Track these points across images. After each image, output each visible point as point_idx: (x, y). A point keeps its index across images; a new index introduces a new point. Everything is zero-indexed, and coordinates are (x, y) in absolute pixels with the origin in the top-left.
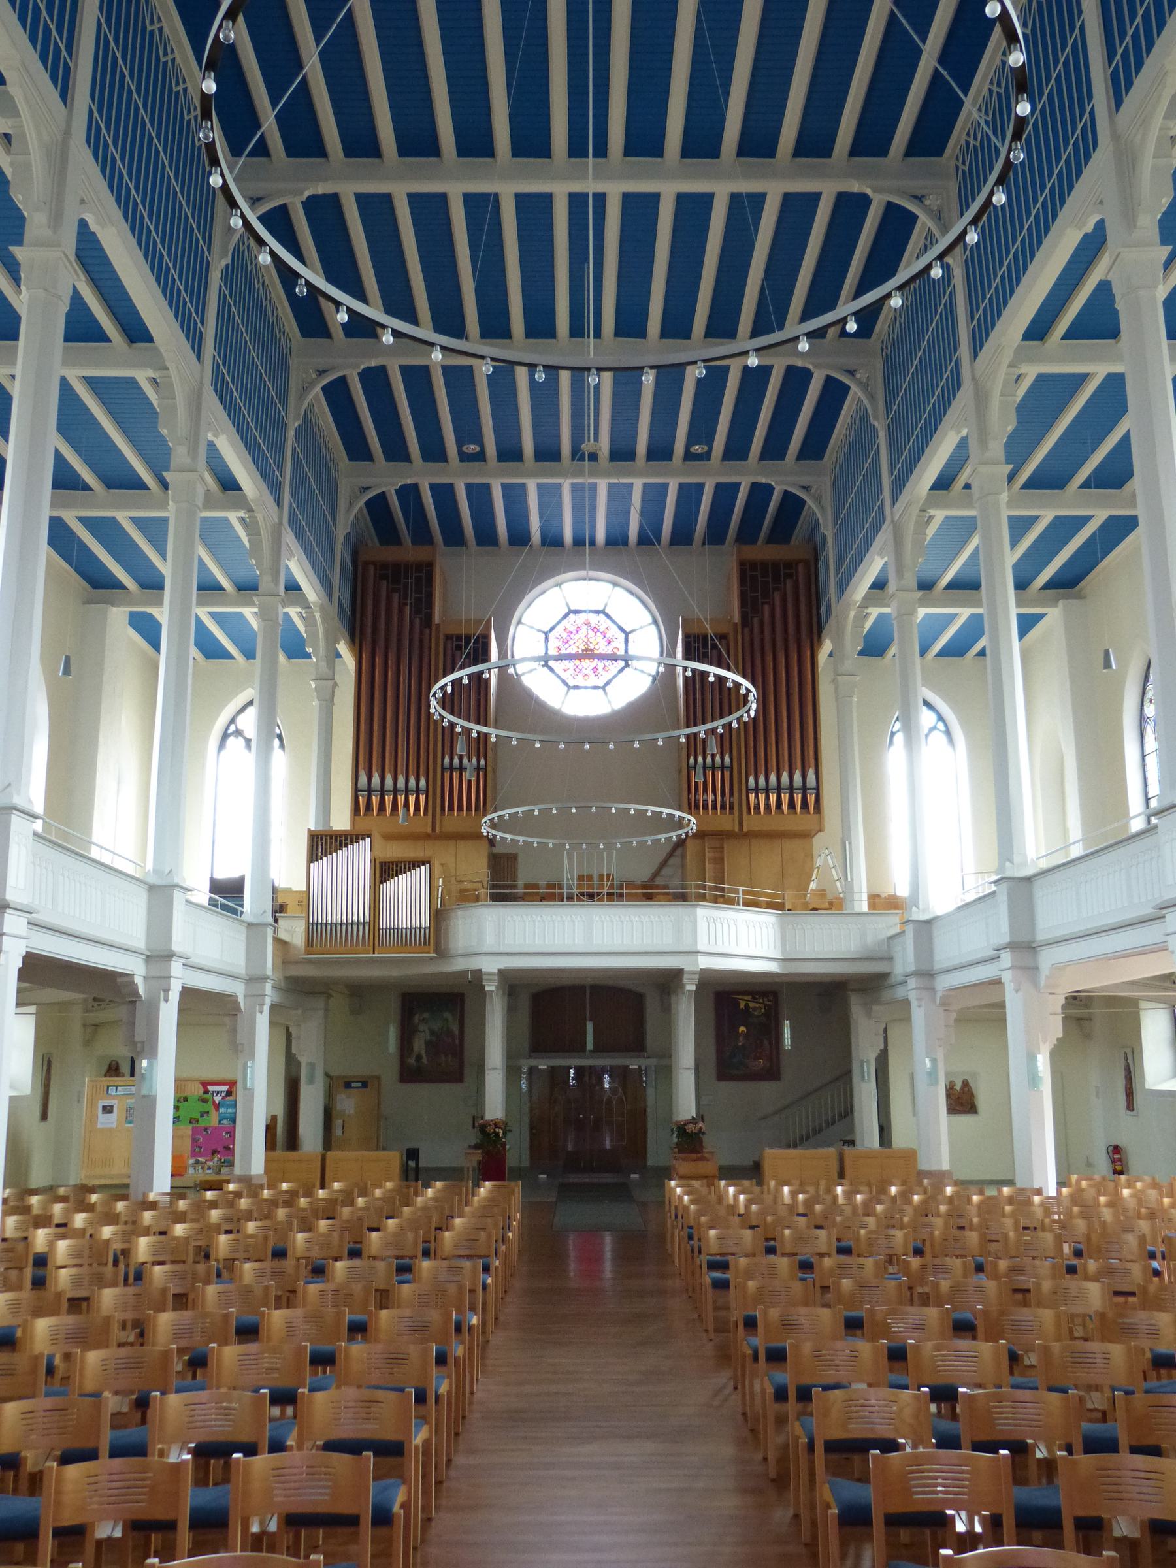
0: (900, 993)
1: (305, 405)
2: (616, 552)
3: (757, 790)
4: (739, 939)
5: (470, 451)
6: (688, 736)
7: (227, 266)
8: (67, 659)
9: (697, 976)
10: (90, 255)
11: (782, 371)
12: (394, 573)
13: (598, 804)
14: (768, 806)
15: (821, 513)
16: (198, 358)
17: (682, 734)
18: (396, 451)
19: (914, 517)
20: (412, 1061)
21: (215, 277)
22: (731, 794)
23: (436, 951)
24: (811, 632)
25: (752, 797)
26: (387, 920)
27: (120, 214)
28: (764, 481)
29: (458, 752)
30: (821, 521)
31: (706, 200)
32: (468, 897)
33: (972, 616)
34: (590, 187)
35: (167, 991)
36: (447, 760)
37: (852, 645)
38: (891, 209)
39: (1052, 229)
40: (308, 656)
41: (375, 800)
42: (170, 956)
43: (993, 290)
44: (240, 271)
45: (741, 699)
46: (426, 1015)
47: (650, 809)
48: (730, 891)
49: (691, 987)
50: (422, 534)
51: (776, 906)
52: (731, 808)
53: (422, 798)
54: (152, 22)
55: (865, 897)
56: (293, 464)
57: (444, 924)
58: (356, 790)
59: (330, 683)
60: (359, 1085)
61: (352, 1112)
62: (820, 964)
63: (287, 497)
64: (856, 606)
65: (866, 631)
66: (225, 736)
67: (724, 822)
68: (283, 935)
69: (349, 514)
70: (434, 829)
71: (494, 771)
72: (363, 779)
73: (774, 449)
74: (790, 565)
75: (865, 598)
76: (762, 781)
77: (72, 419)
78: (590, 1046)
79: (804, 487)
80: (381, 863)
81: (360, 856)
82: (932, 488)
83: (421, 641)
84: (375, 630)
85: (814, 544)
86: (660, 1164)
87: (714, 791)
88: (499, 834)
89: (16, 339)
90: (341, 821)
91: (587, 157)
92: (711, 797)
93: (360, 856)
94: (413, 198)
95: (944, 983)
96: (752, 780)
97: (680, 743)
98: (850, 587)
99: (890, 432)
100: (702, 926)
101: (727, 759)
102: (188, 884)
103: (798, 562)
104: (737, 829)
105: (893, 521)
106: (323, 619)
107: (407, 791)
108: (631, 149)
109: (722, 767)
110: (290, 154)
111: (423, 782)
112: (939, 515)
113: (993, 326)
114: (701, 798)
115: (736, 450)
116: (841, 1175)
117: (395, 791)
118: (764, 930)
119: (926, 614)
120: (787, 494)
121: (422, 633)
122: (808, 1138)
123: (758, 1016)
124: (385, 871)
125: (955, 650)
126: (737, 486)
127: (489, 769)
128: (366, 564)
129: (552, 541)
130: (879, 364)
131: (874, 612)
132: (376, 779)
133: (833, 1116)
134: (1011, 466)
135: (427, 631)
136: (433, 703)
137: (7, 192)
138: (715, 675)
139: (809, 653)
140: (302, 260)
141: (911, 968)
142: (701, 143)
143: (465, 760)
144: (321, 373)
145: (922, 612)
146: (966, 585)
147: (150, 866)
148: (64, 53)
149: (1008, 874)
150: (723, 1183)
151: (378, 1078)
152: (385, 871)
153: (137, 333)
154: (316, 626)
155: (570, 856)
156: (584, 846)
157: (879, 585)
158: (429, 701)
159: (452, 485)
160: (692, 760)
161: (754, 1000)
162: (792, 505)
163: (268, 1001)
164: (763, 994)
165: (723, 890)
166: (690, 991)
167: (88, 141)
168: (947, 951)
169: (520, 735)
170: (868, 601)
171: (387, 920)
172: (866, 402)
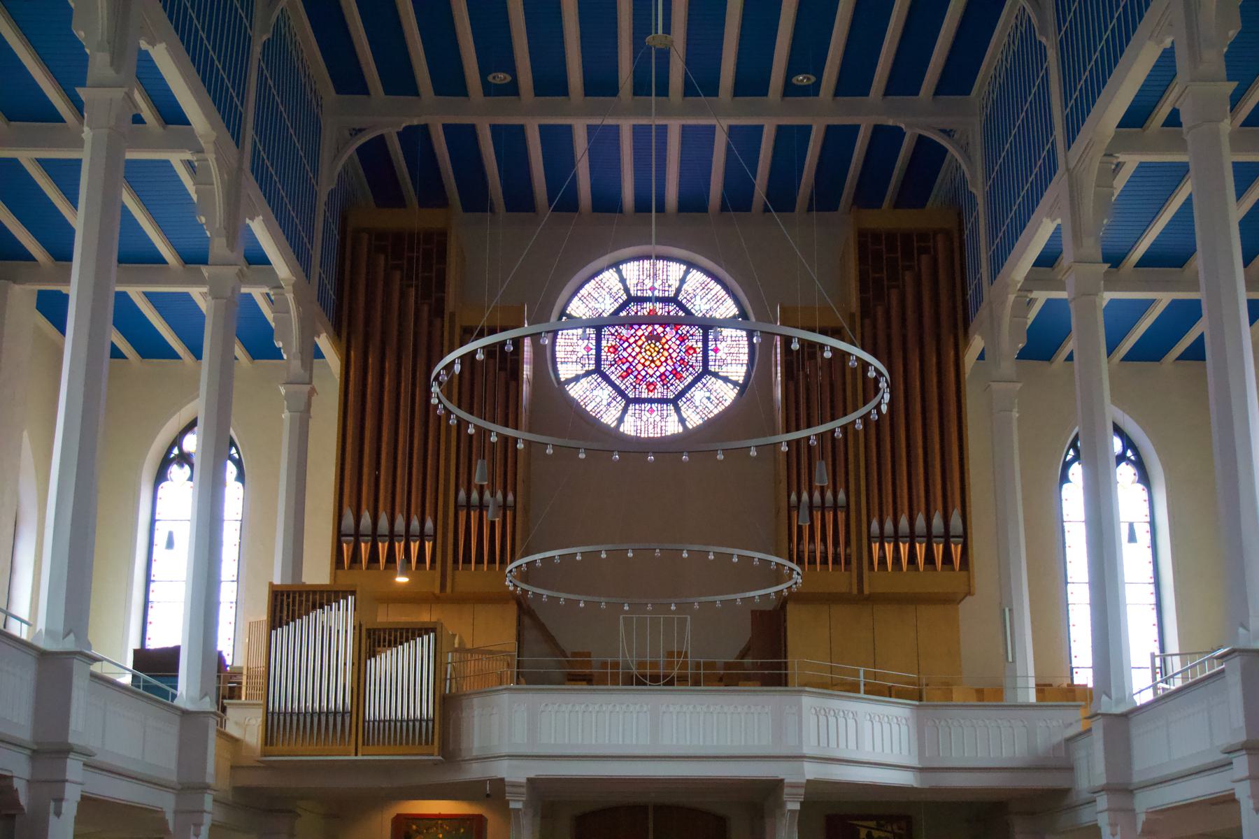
0: (1086, 816)
1: (277, 12)
2: (695, 217)
3: (882, 539)
5: (497, 81)
9: (802, 791)
12: (394, 245)
13: (677, 600)
15: (969, 167)
17: (783, 439)
18: (399, 80)
19: (1096, 166)
22: (847, 544)
24: (955, 326)
25: (875, 547)
26: (376, 708)
28: (891, 123)
29: (477, 480)
32: (490, 684)
33: (1174, 304)
35: (59, 800)
36: (462, 494)
37: (1011, 341)
39: (1146, 15)
40: (277, 354)
41: (364, 548)
42: (64, 751)
43: (1110, 27)
45: (871, 386)
47: (736, 553)
50: (432, 194)
51: (913, 693)
52: (848, 562)
53: (428, 546)
55: (1032, 683)
58: (339, 535)
59: (307, 388)
62: (964, 775)
64: (1013, 292)
65: (1030, 322)
66: (165, 463)
67: (838, 580)
68: (231, 729)
69: (334, 165)
70: (443, 587)
71: (526, 510)
72: (349, 520)
73: (904, 81)
79: (943, 131)
80: (368, 630)
81: (340, 621)
82: (1119, 126)
83: (430, 334)
84: (368, 321)
85: (959, 204)
87: (824, 540)
88: (532, 589)
90: (318, 572)
92: (819, 547)
93: (340, 621)
95: (1146, 802)
96: (875, 525)
98: (1007, 264)
99: (1062, 48)
100: (810, 721)
101: (841, 496)
102: (95, 652)
104: (855, 591)
105: (1068, 170)
106: (298, 302)
107: (408, 537)
109: (835, 507)
111: (429, 524)
112: (1131, 162)
113: (1135, 29)
114: (806, 547)
115: (854, 81)
117: (392, 536)
118: (895, 727)
119: (1112, 301)
120: (921, 139)
121: (431, 324)
124: (373, 640)
125: (1150, 351)
126: (856, 128)
127: (519, 506)
131: (1041, 297)
132: (366, 519)
134: (1234, 84)
135: (437, 322)
136: (435, 389)
138: (833, 349)
139: (952, 353)
141: (1101, 780)
143: (487, 495)
145: (1108, 296)
146: (1170, 258)
147: (41, 625)
149: (1241, 644)
152: (373, 640)
153: (172, 115)
154: (288, 312)
155: (628, 622)
156: (649, 607)
157: (1048, 260)
158: (429, 387)
159: (473, 127)
160: (794, 497)
162: (929, 156)
163: (207, 820)
166: (792, 812)
168: (1154, 754)
169: (559, 442)
170: (1032, 282)
171: (376, 708)
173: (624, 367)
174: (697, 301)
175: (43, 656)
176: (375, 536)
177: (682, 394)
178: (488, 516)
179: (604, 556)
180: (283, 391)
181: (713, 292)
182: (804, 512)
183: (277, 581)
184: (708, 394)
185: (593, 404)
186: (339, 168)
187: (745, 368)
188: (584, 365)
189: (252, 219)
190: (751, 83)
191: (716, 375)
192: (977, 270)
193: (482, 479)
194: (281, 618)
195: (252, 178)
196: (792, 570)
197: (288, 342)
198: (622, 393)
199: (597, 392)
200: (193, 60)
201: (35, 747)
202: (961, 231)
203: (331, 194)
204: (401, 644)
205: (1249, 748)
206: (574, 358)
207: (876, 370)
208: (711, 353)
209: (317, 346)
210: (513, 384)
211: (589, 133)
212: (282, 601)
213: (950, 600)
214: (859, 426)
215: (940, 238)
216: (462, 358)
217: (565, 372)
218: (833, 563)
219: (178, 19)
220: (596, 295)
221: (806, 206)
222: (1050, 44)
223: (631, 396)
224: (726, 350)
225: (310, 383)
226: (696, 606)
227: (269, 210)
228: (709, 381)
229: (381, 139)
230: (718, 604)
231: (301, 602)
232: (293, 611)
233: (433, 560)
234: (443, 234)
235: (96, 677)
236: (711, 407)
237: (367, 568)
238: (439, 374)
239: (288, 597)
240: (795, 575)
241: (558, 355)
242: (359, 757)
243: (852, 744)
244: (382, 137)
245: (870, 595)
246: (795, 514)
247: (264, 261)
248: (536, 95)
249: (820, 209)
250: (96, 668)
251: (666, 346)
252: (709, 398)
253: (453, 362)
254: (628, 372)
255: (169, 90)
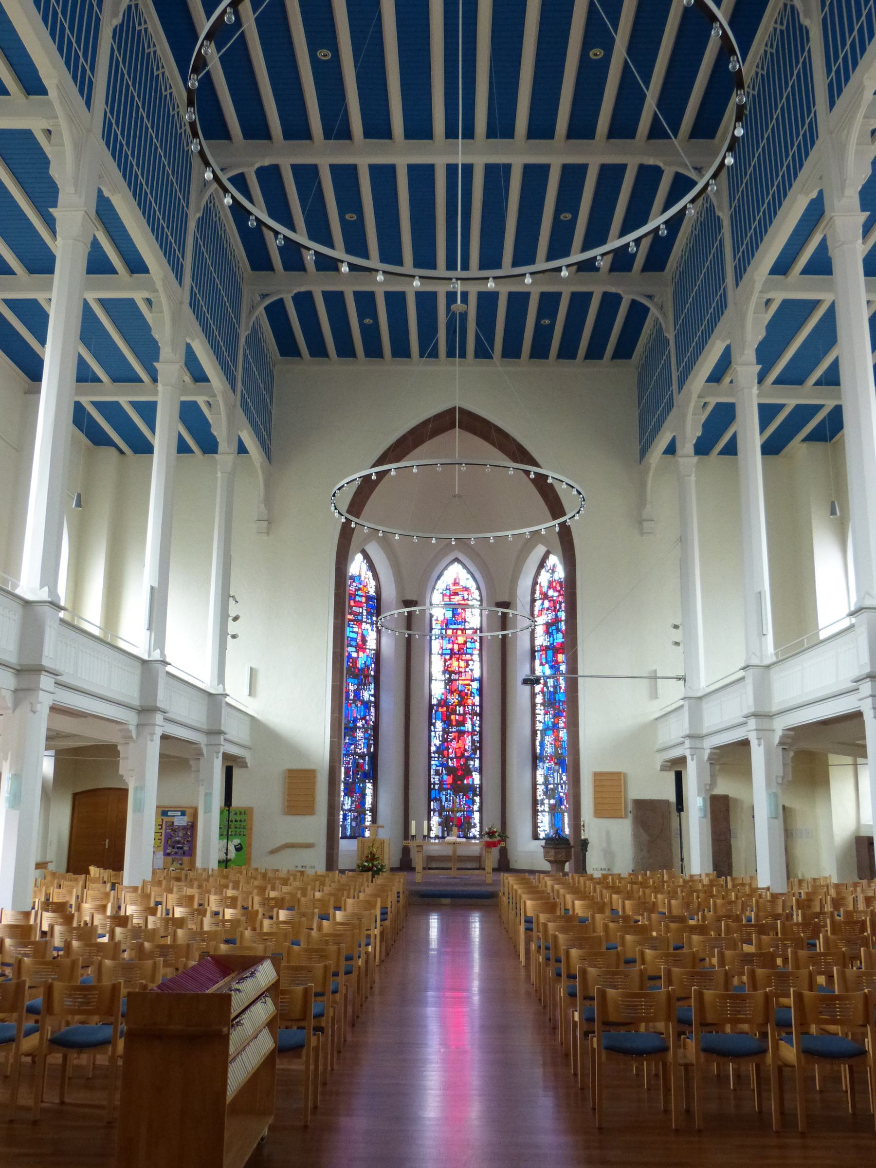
1: (253, 319)
6: (503, 635)
7: (199, 219)
8: (79, 496)
10: (105, 212)
11: (635, 170)
16: (180, 284)
21: (192, 225)
27: (120, 174)
31: (545, 169)
34: (460, 160)
38: (634, 303)
42: (38, 669)
44: (208, 222)
54: (158, 69)
56: (244, 362)
63: (239, 385)
77: (90, 331)
82: (707, 381)
89: (52, 271)
91: (457, 137)
94: (334, 168)
108: (491, 133)
110: (311, 355)
130: (670, 290)
137: (48, 172)
140: (251, 201)
142: (541, 129)
144: (264, 296)
148: (88, 72)
153: (137, 266)
159: (342, 293)
167: (103, 138)
172: (661, 320)
175: (144, 662)
189: (242, 431)
190: (541, 129)
195: (241, 410)
201: (19, 668)
205: (872, 677)
222: (724, 215)
229: (281, 301)
235: (168, 673)
244: (281, 300)
247: (207, 380)
248: (365, 137)
250: (169, 668)
255: (137, 251)
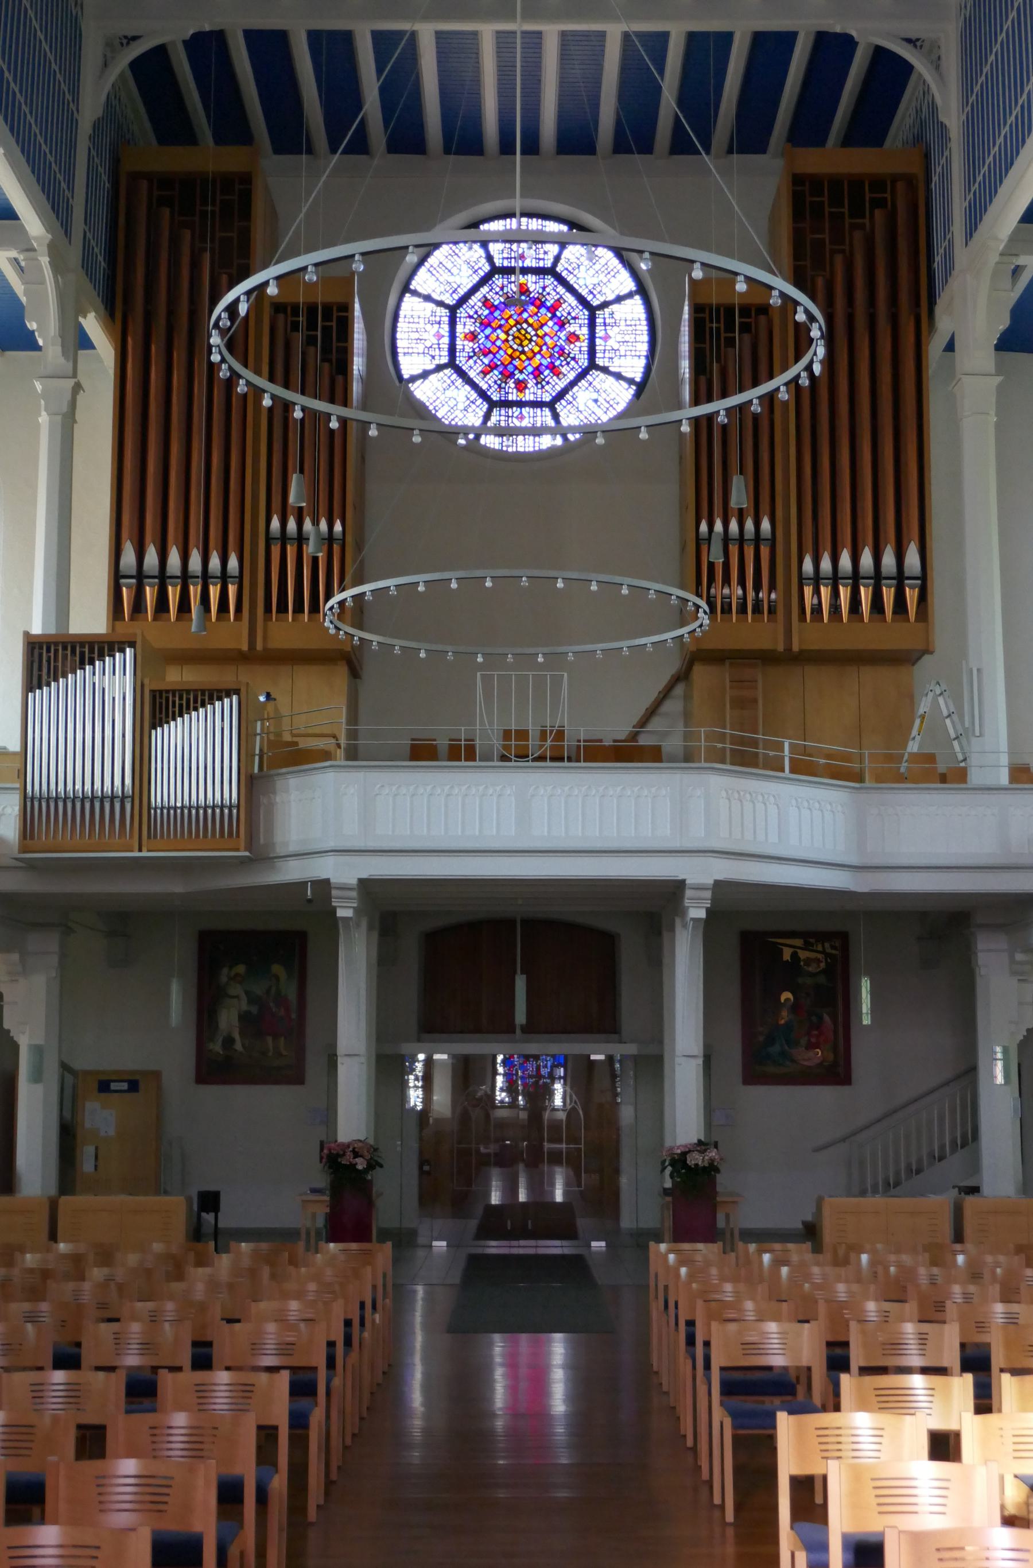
4: (786, 829)
9: (708, 894)
12: (181, 193)
13: (546, 650)
14: (835, 608)
20: (216, 1047)
23: (249, 847)
24: (917, 304)
25: (808, 591)
30: (938, 100)
41: (150, 594)
46: (241, 969)
48: (768, 745)
49: (698, 913)
50: (232, 127)
52: (772, 611)
53: (232, 590)
57: (264, 800)
58: (117, 576)
60: (125, 1086)
61: (112, 1132)
69: (99, 85)
72: (129, 557)
74: (878, 183)
75: (1014, 238)
76: (826, 564)
78: (520, 1017)
79: (909, 41)
80: (153, 693)
81: (116, 681)
85: (926, 142)
86: (642, 1225)
90: (90, 618)
93: (116, 681)
97: (682, 435)
103: (895, 178)
111: (233, 563)
116: (959, 1237)
122: (897, 1184)
123: (813, 975)
124: (158, 707)
127: (349, 539)
128: (135, 177)
129: (464, 140)
132: (151, 558)
133: (942, 1147)
136: (215, 339)
138: (749, 280)
143: (308, 525)
150: (752, 1247)
151: (156, 1075)
152: (158, 707)
154: (43, 282)
155: (487, 680)
160: (704, 527)
161: (807, 946)
164: (823, 936)
165: (755, 743)
166: (695, 920)
173: (486, 361)
174: (582, 273)
176: (163, 577)
177: (561, 395)
178: (310, 549)
179: (454, 585)
180: (39, 386)
181: (603, 261)
182: (717, 547)
183: (37, 629)
184: (595, 396)
185: (446, 408)
186: (107, 87)
187: (643, 362)
188: (433, 357)
191: (605, 370)
192: (948, 221)
193: (299, 498)
194: (40, 677)
196: (698, 607)
197: (44, 324)
198: (483, 395)
199: (452, 392)
200: (12, 130)
202: (928, 180)
203: (97, 126)
204: (196, 709)
206: (421, 348)
207: (807, 311)
208: (598, 341)
209: (80, 325)
210: (340, 378)
211: (437, 38)
212: (41, 655)
213: (904, 659)
214: (783, 395)
215: (900, 186)
216: (248, 293)
217: (409, 366)
218: (753, 612)
219: (13, 120)
220: (449, 265)
221: (725, 147)
223: (495, 397)
224: (619, 338)
225: (75, 375)
226: (571, 657)
227: (13, 141)
228: (597, 377)
230: (599, 654)
231: (65, 657)
232: (56, 668)
233: (239, 609)
234: (246, 180)
236: (599, 412)
237: (155, 619)
238: (219, 318)
239: (48, 650)
240: (701, 614)
241: (399, 343)
242: (145, 854)
243: (773, 838)
245: (801, 652)
246: (704, 548)
249: (742, 151)
251: (540, 333)
252: (596, 401)
253: (237, 301)
254: (492, 367)
